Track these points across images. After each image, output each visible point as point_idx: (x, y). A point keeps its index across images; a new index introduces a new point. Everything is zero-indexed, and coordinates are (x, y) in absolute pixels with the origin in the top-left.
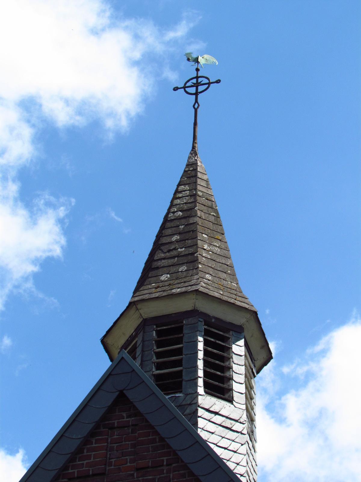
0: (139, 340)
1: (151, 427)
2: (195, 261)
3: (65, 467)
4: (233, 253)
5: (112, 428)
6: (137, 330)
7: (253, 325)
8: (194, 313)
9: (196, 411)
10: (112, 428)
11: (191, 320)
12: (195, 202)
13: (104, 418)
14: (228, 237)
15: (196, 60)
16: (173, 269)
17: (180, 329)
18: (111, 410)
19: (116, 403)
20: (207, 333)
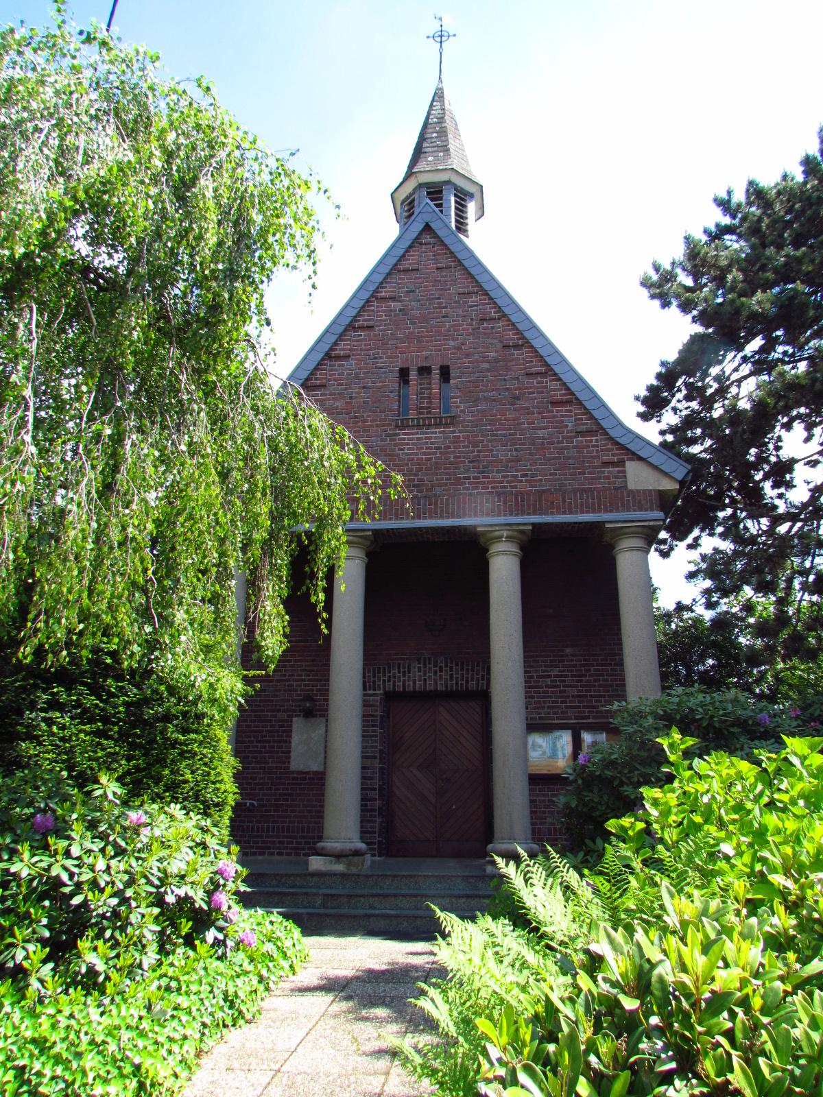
0: (416, 196)
1: (446, 245)
2: (448, 150)
3: (396, 265)
4: (466, 148)
5: (421, 244)
6: (415, 190)
7: (479, 195)
8: (448, 182)
9: (762, 198)
10: (421, 244)
11: (447, 187)
12: (444, 113)
13: (418, 238)
14: (463, 137)
15: (440, 19)
16: (435, 154)
17: (441, 192)
18: (421, 233)
19: (424, 230)
20: (456, 196)
